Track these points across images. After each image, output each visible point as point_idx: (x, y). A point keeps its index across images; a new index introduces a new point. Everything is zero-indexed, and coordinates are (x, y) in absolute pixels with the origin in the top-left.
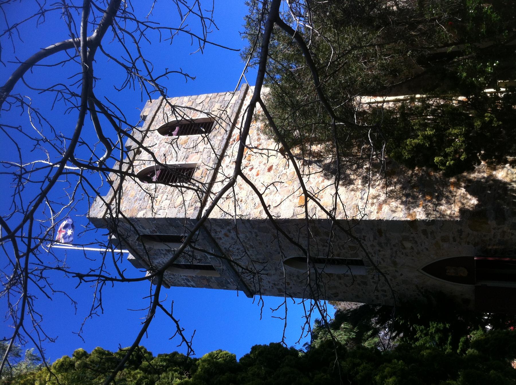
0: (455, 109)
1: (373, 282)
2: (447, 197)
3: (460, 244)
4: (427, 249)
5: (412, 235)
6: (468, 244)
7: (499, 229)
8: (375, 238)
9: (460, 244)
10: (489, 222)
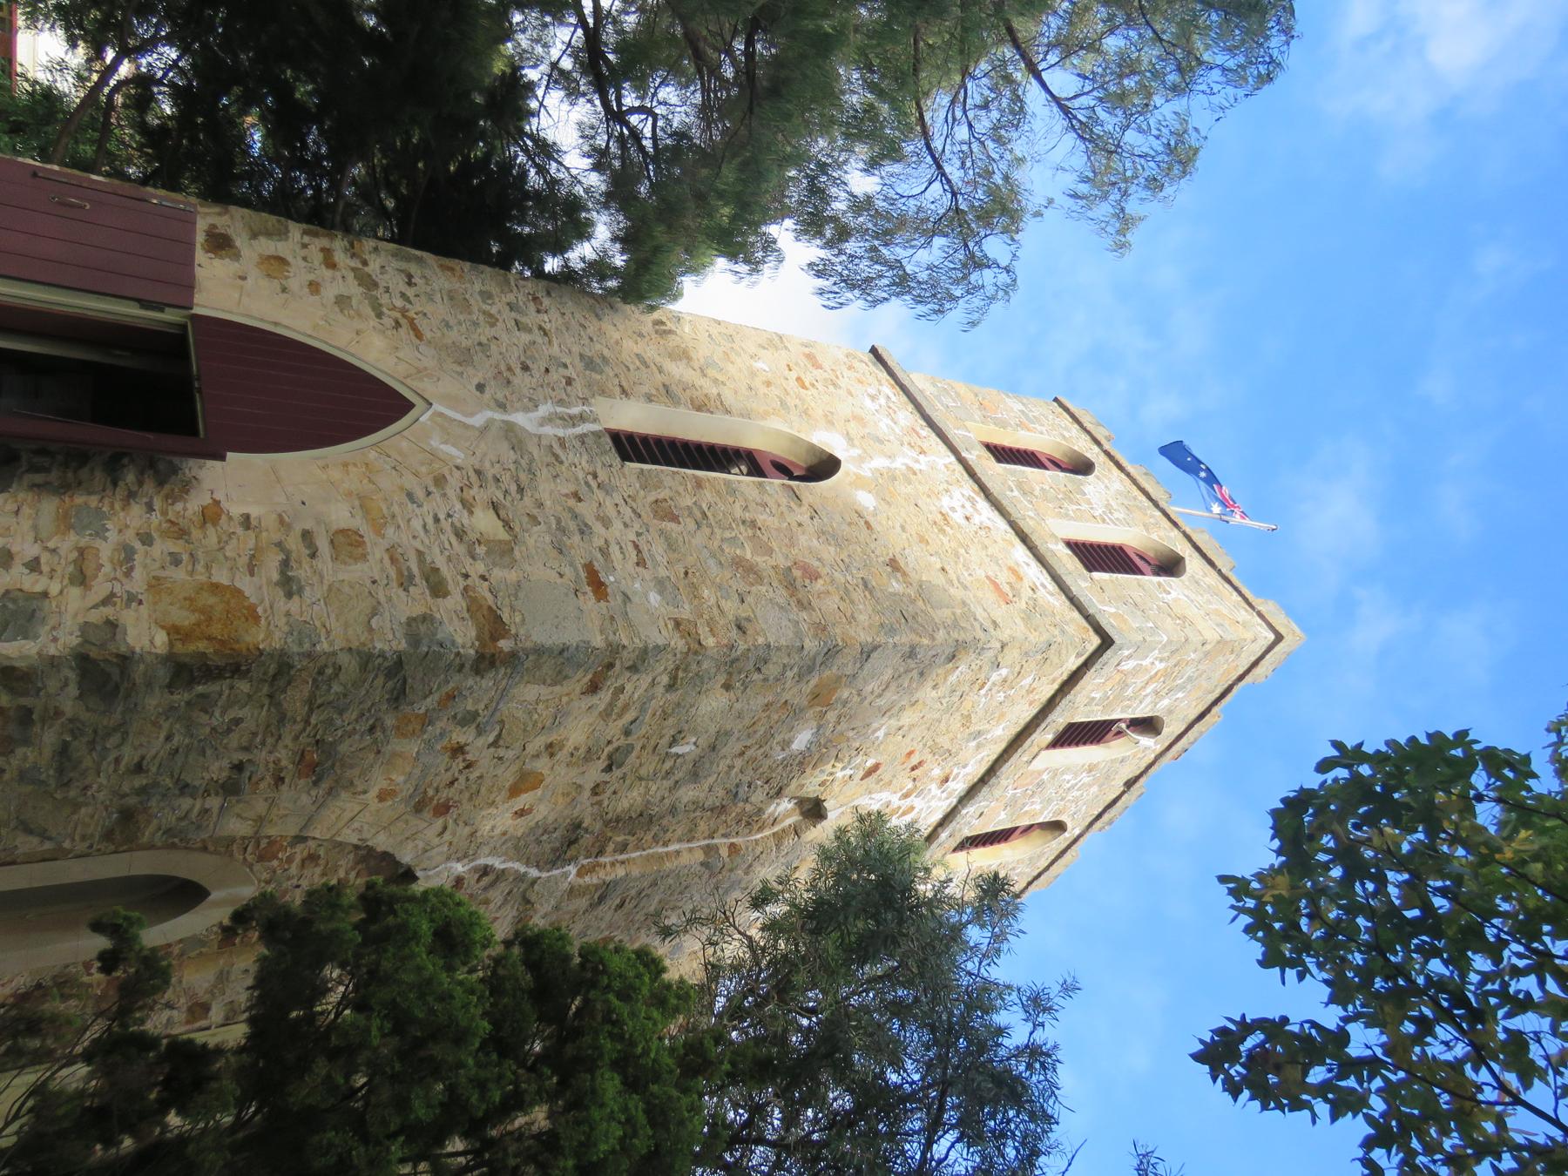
0: (319, 964)
1: (565, 366)
2: (970, 1007)
3: (281, 521)
4: (410, 495)
5: (480, 568)
6: (247, 517)
7: (108, 600)
8: (604, 551)
9: (281, 521)
10: (161, 638)
